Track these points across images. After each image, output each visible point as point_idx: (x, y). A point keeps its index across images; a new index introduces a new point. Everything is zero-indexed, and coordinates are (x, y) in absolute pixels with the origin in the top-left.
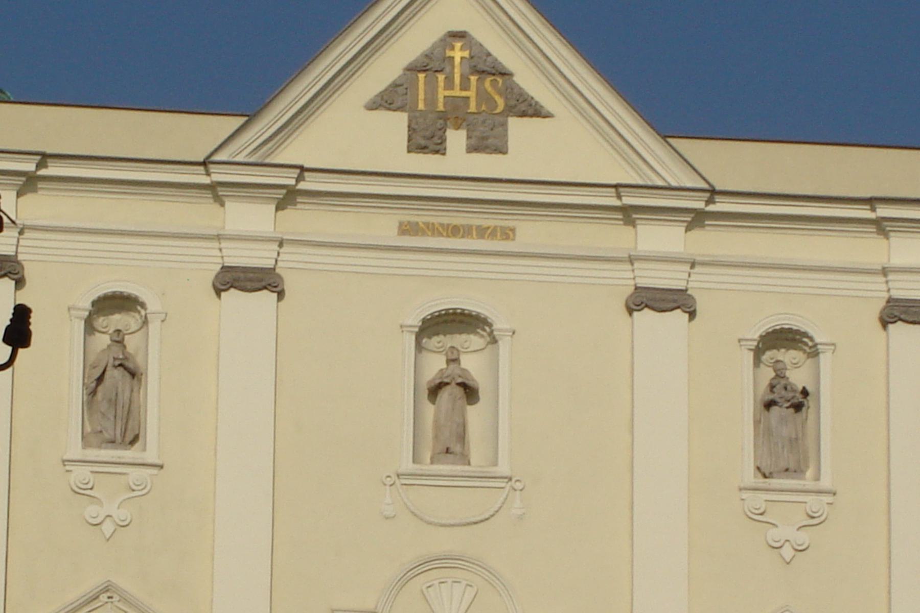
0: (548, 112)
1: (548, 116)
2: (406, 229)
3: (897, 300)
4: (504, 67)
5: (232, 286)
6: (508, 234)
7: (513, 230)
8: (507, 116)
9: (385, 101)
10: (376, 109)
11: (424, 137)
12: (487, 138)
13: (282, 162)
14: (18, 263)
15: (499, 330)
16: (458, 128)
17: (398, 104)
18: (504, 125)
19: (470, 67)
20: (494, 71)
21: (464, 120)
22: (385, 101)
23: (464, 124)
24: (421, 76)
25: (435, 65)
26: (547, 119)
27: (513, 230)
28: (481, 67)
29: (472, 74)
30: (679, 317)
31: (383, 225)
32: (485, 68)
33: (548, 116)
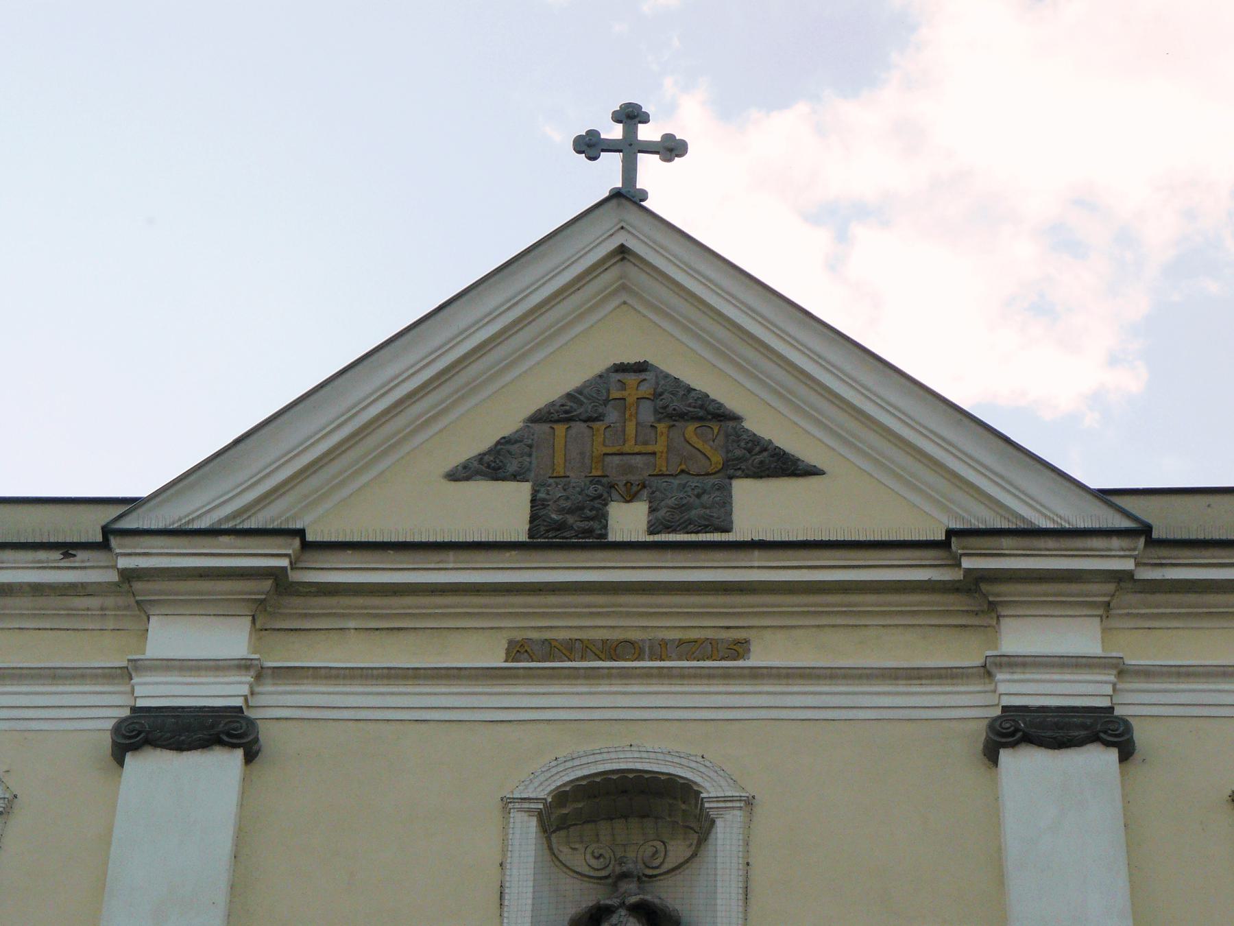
0: (808, 465)
1: (812, 472)
2: (517, 650)
3: (142, 709)
4: (721, 405)
5: (135, 748)
6: (739, 649)
7: (747, 642)
8: (731, 478)
9: (492, 465)
10: (467, 479)
11: (561, 511)
12: (689, 507)
13: (154, 526)
14: (251, 723)
15: (717, 799)
16: (630, 498)
17: (512, 467)
18: (726, 491)
19: (656, 412)
20: (701, 413)
21: (644, 487)
22: (492, 465)
23: (645, 493)
24: (560, 429)
25: (587, 409)
26: (813, 481)
27: (747, 642)
28: (678, 405)
29: (659, 421)
30: (1102, 759)
31: (56, 555)
32: (685, 409)
33: (812, 472)
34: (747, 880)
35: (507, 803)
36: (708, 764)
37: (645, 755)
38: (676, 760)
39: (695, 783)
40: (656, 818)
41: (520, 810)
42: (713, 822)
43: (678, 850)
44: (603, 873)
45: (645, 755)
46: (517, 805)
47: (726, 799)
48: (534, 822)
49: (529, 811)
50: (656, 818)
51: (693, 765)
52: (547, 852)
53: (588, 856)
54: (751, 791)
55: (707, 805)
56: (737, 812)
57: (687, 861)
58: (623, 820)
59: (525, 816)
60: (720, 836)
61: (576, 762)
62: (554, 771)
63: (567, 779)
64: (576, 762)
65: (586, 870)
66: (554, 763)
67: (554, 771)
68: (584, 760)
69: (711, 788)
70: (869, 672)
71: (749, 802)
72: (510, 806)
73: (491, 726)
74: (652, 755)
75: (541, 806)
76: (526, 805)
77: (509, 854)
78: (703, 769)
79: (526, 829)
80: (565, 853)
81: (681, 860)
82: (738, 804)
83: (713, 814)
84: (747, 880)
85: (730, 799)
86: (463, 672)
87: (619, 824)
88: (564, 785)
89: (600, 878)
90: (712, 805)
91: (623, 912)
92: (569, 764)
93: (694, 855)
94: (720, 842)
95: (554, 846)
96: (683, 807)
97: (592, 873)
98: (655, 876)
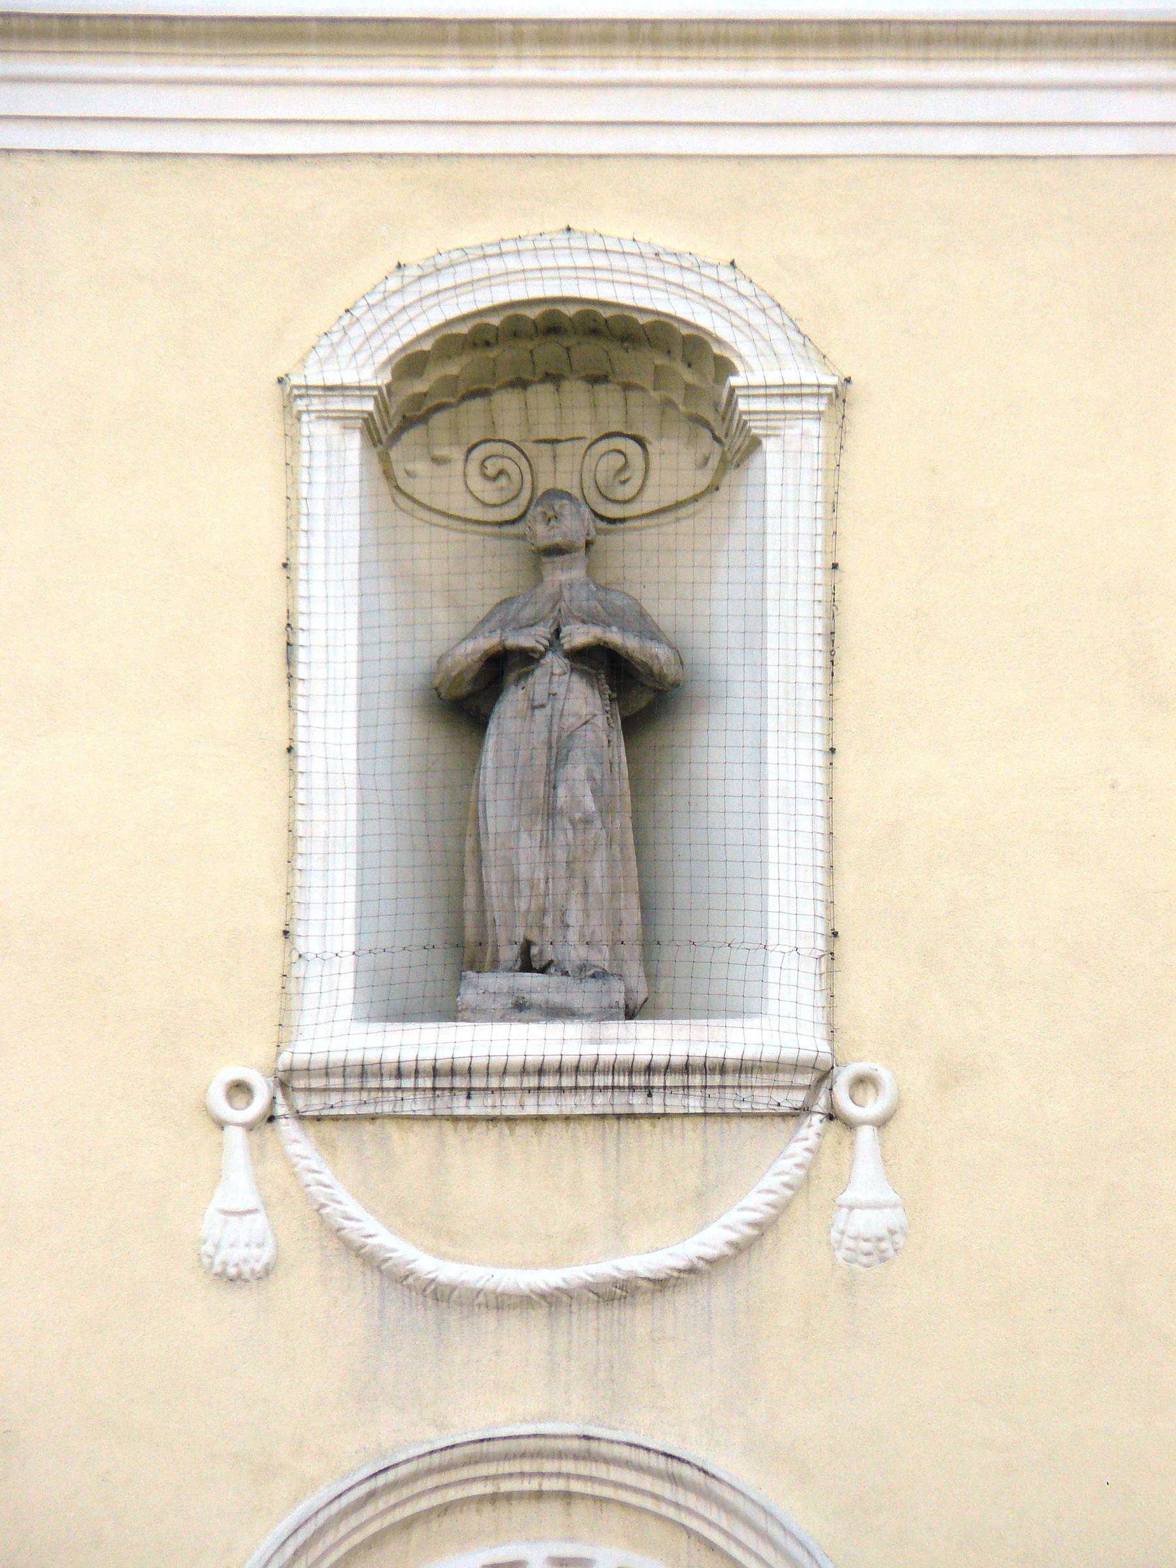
15: (766, 391)
34: (833, 607)
35: (292, 396)
36: (744, 288)
37: (600, 261)
38: (674, 276)
39: (719, 341)
40: (627, 387)
41: (324, 416)
42: (755, 443)
43: (674, 466)
44: (510, 513)
45: (600, 261)
46: (317, 405)
47: (787, 391)
48: (354, 442)
49: (343, 418)
50: (627, 387)
51: (712, 290)
52: (384, 487)
53: (473, 468)
54: (847, 376)
55: (742, 405)
56: (812, 427)
57: (695, 499)
58: (549, 387)
59: (334, 428)
60: (773, 476)
61: (446, 281)
62: (396, 302)
63: (422, 327)
64: (446, 281)
65: (460, 504)
66: (393, 283)
67: (396, 302)
68: (463, 274)
69: (760, 363)
70: (1113, 30)
71: (839, 395)
72: (301, 404)
73: (249, 168)
74: (618, 262)
75: (369, 406)
76: (336, 404)
77: (303, 540)
78: (736, 305)
79: (337, 460)
80: (425, 479)
81: (683, 494)
82: (810, 405)
83: (756, 427)
84: (833, 607)
85: (795, 391)
86: (178, 27)
87: (542, 396)
88: (419, 339)
89: (501, 524)
90: (758, 405)
91: (555, 663)
92: (430, 285)
93: (714, 488)
94: (773, 492)
95: (399, 471)
96: (688, 376)
97: (478, 513)
98: (622, 520)
